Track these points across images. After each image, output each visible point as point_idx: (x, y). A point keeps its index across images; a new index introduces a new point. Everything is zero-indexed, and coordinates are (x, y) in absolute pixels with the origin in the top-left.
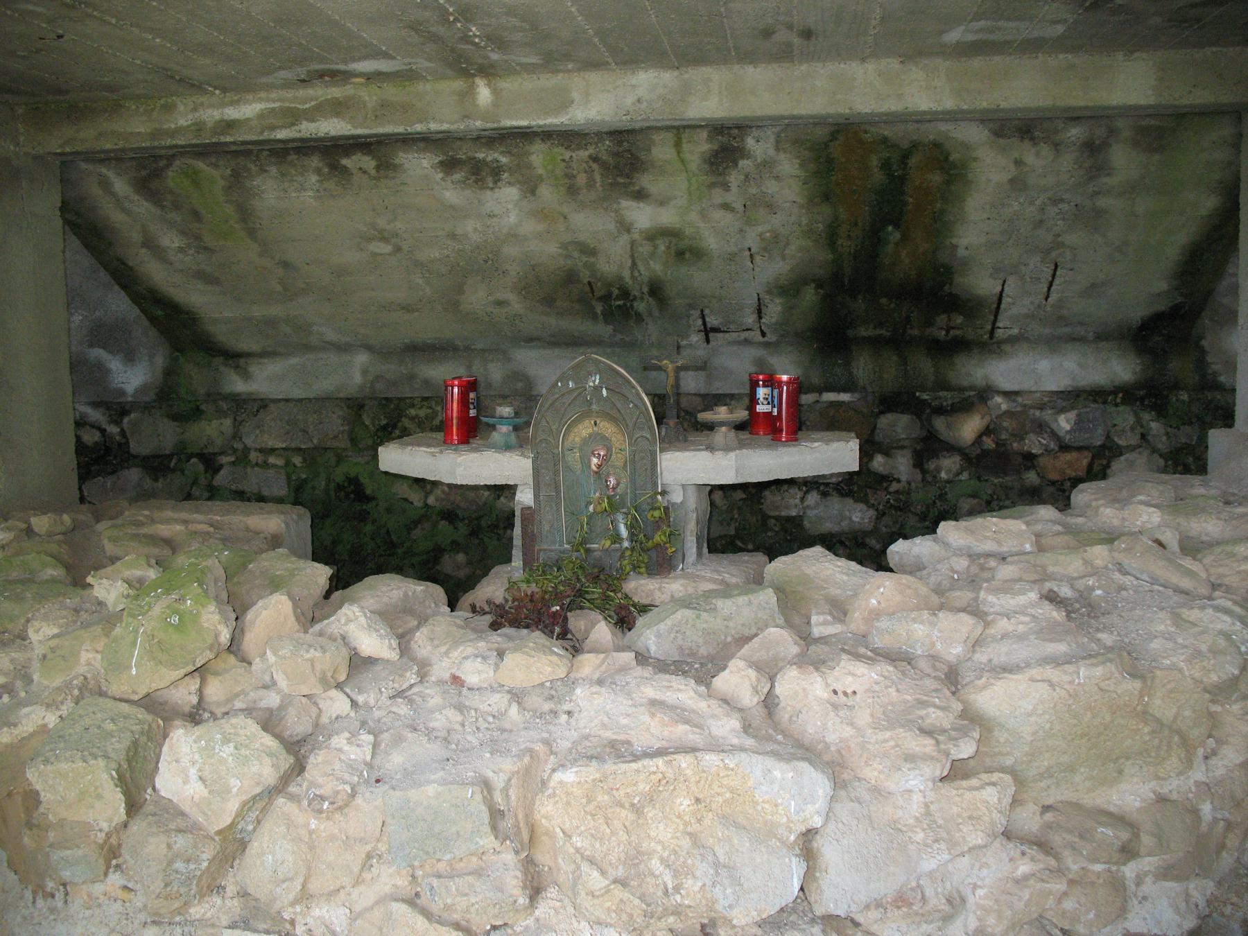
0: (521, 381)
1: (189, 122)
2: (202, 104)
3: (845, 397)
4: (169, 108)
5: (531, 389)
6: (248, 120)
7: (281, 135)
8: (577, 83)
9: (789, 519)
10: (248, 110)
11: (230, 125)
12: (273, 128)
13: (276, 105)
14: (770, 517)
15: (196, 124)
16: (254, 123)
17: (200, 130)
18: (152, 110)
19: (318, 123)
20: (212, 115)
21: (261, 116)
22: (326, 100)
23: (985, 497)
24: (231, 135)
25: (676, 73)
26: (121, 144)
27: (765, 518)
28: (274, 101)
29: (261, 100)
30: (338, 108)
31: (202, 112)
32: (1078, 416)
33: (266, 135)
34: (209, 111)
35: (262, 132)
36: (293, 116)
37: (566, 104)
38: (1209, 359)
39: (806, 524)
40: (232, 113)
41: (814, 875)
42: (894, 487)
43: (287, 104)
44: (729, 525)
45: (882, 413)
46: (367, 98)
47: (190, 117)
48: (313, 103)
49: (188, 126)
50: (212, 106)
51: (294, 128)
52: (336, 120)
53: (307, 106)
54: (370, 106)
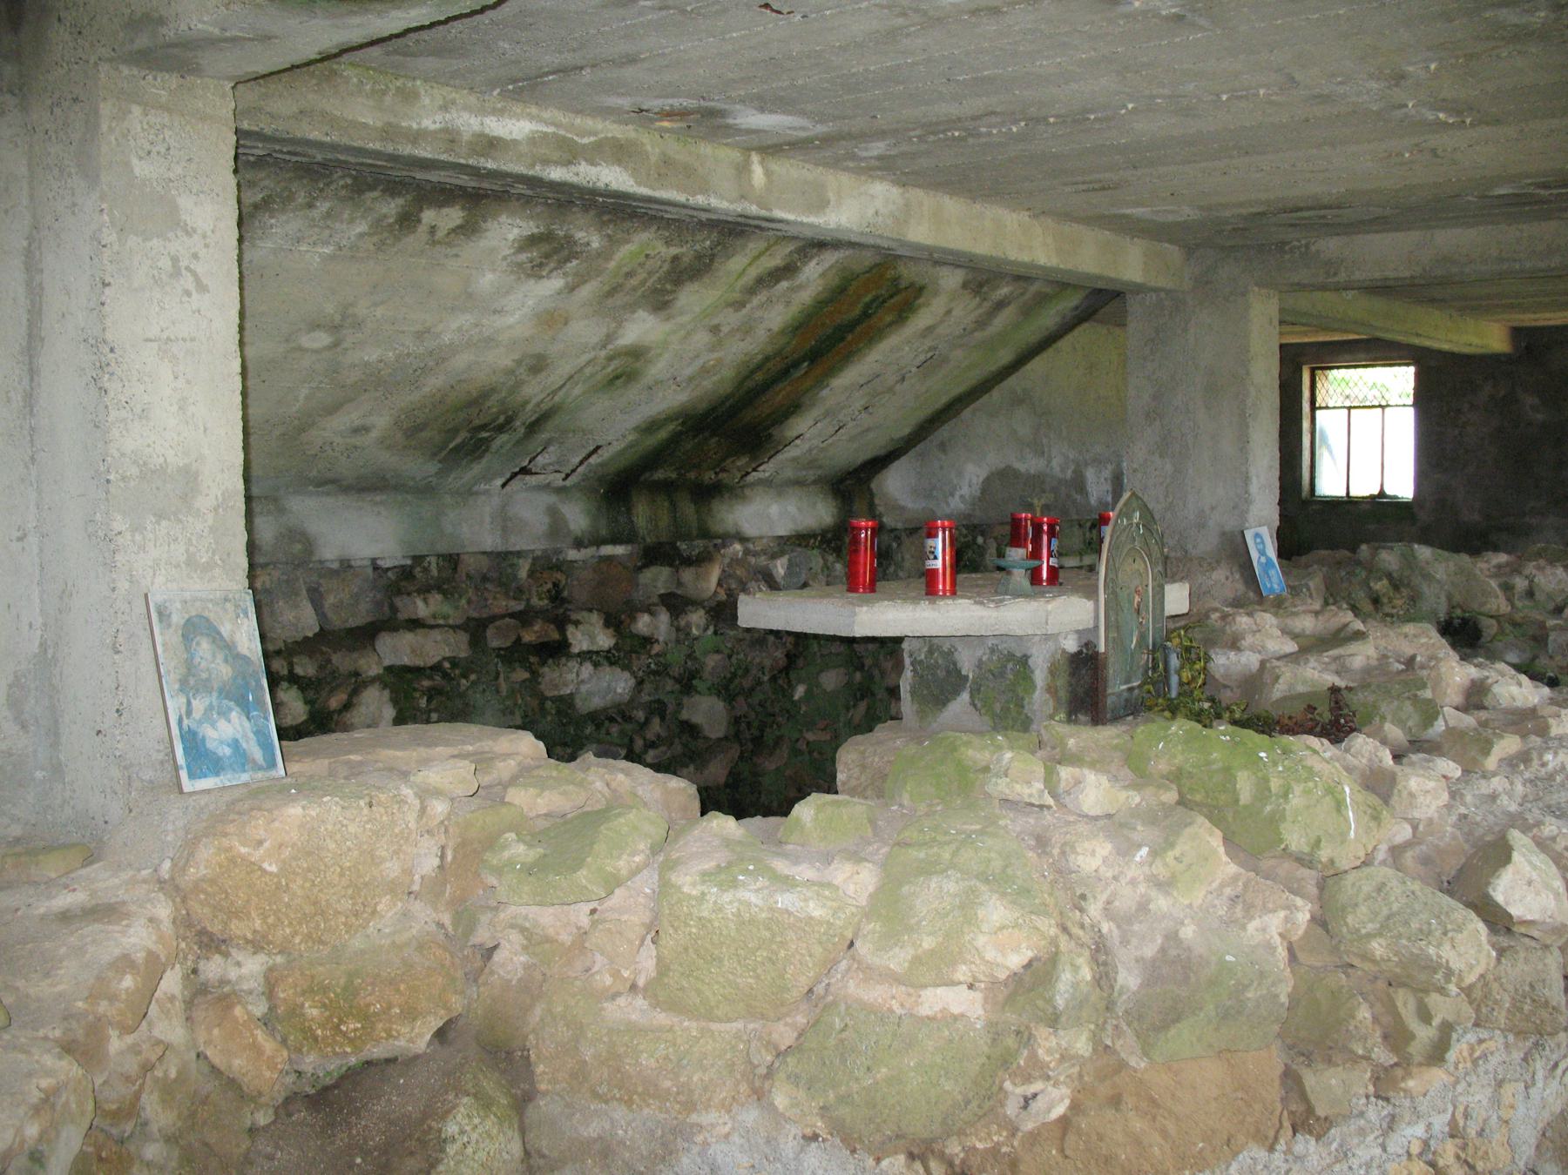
0: (299, 542)
1: (438, 126)
2: (453, 102)
3: (619, 550)
4: (409, 96)
5: (311, 553)
6: (515, 142)
7: (556, 174)
8: (836, 181)
9: (561, 699)
10: (515, 127)
11: (492, 144)
12: (546, 162)
13: (551, 130)
14: (547, 698)
15: (446, 130)
16: (524, 149)
17: (452, 141)
18: (384, 93)
19: (599, 168)
20: (470, 123)
21: (533, 140)
22: (606, 138)
23: (727, 651)
24: (494, 159)
25: (901, 190)
26: (334, 137)
27: (543, 699)
28: (547, 123)
29: (531, 118)
30: (619, 152)
31: (455, 115)
32: (789, 560)
33: (537, 171)
34: (466, 115)
35: (533, 166)
36: (570, 153)
37: (822, 205)
38: (877, 501)
39: (578, 702)
40: (498, 127)
41: (1147, 984)
42: (656, 649)
43: (562, 132)
44: (512, 713)
45: (645, 566)
46: (649, 148)
47: (438, 118)
48: (592, 139)
49: (435, 132)
50: (466, 108)
51: (573, 168)
52: (618, 169)
53: (586, 141)
54: (653, 159)
